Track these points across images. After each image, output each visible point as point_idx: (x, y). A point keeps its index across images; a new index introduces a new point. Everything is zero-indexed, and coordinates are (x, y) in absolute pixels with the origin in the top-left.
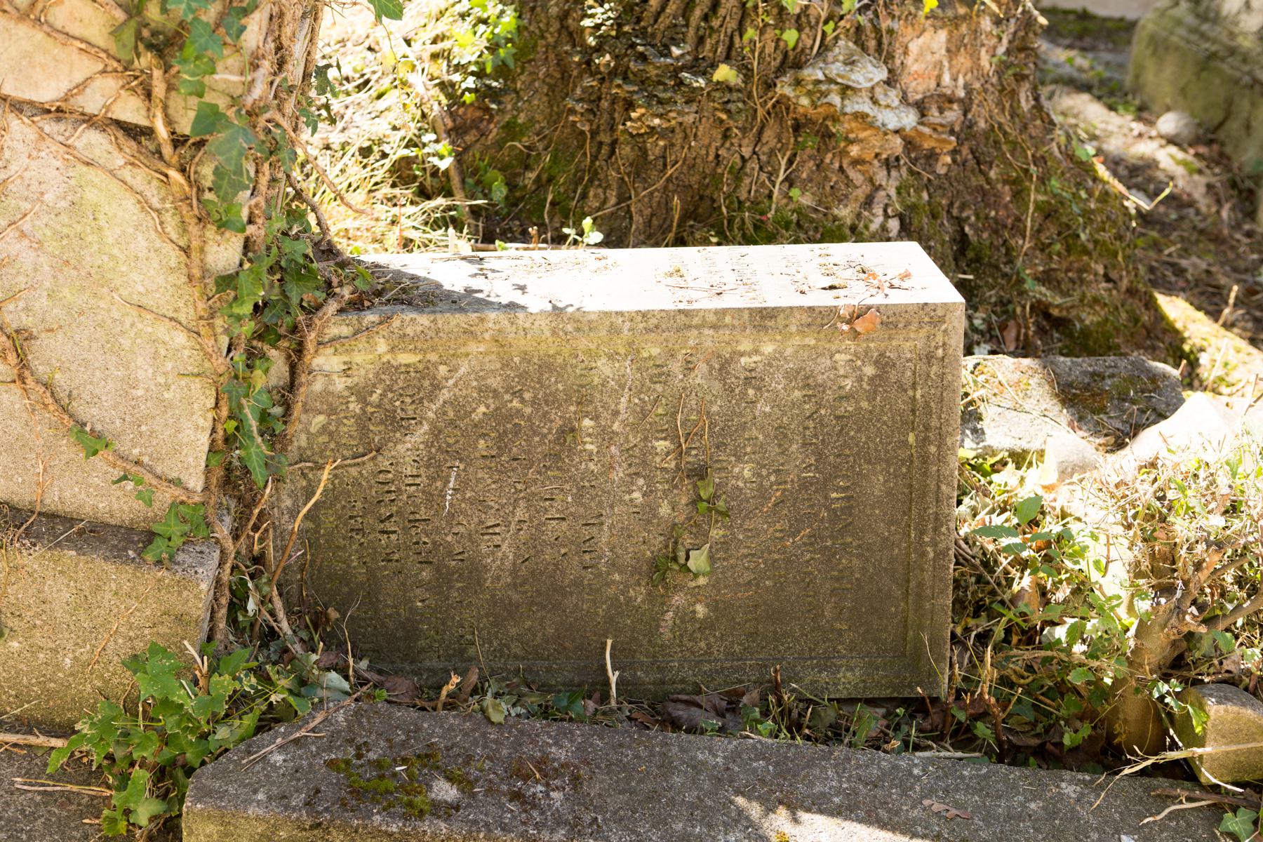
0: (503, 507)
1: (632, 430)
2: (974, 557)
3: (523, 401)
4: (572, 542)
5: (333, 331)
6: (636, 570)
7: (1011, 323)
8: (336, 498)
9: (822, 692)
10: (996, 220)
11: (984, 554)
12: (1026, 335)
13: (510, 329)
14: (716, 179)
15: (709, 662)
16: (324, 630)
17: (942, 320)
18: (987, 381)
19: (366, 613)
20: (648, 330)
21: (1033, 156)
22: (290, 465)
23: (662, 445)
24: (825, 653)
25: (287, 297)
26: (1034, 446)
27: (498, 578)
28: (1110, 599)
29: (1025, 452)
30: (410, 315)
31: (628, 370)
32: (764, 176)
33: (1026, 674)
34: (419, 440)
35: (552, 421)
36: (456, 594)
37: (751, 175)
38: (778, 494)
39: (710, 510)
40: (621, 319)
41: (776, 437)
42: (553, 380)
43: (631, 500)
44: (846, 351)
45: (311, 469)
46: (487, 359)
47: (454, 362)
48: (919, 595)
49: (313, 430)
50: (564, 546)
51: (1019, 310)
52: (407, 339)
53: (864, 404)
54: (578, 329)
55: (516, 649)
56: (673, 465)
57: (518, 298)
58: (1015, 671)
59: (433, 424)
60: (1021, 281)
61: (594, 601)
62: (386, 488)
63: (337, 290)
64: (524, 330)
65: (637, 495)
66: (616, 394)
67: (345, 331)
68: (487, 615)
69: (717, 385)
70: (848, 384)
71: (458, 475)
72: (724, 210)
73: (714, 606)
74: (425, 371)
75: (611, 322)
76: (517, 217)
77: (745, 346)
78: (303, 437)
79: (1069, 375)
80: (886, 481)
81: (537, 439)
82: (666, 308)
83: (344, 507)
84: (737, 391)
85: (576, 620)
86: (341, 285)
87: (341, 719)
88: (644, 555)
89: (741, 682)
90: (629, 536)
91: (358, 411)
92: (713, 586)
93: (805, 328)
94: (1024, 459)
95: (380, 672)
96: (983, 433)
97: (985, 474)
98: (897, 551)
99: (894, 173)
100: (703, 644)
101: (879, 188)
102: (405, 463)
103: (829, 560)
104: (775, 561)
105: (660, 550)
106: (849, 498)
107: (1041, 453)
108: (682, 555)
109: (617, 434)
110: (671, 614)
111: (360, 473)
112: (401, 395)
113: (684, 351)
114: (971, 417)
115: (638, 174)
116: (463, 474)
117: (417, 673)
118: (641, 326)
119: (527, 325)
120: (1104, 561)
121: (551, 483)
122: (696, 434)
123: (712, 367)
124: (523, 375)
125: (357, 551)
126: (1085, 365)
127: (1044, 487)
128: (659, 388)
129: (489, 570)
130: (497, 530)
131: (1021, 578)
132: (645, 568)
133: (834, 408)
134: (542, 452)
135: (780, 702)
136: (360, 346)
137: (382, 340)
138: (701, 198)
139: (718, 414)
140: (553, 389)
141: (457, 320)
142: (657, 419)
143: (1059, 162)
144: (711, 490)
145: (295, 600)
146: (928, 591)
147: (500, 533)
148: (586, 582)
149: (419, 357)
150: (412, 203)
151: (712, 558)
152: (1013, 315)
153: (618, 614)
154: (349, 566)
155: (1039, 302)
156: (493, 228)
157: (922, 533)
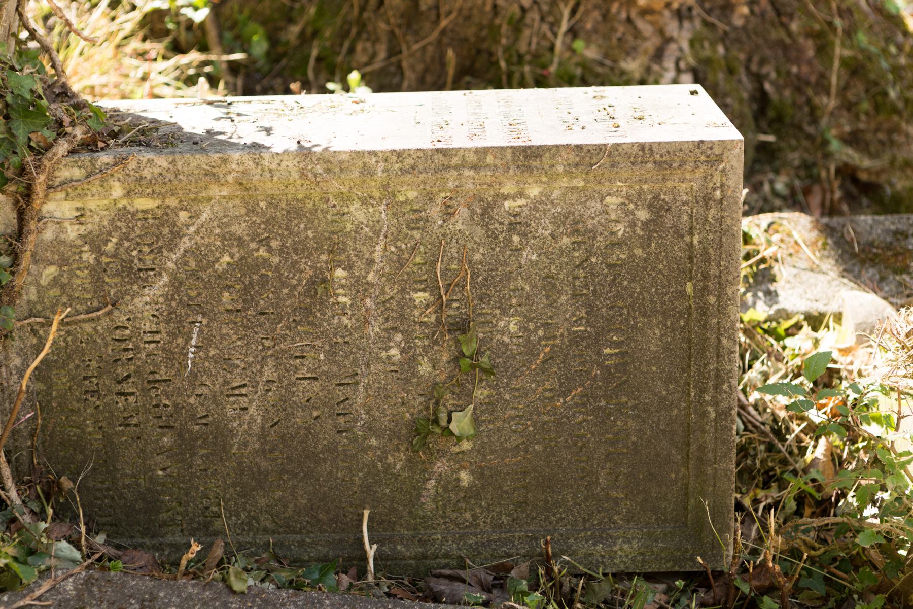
0: (250, 365)
1: (388, 280)
2: (763, 424)
3: (270, 250)
4: (325, 404)
5: (65, 173)
6: (394, 434)
7: (816, 189)
8: (69, 357)
9: (598, 567)
10: (798, 77)
11: (775, 421)
12: (832, 201)
13: (255, 171)
14: (494, 31)
15: (475, 535)
16: (57, 502)
17: (719, 159)
18: (782, 241)
19: (102, 482)
20: (404, 171)
21: (839, 8)
22: (19, 320)
23: (420, 297)
24: (599, 524)
25: (13, 135)
26: (832, 308)
27: (245, 444)
28: (901, 455)
29: (822, 315)
30: (147, 155)
31: (383, 216)
32: (545, 28)
33: (816, 545)
34: (158, 293)
35: (301, 272)
36: (200, 462)
37: (532, 26)
38: (547, 350)
39: (473, 367)
40: (374, 160)
41: (543, 288)
42: (302, 226)
43: (389, 358)
44: (617, 194)
45: (42, 325)
46: (231, 204)
47: (195, 207)
48: (700, 459)
49: (43, 282)
50: (317, 408)
51: (824, 174)
52: (144, 182)
53: (638, 252)
54: (328, 171)
55: (266, 521)
56: (433, 318)
57: (262, 138)
58: (805, 542)
59: (173, 275)
60: (825, 143)
61: (350, 469)
62: (123, 346)
63: (69, 130)
64: (270, 171)
65: (394, 352)
66: (371, 242)
67: (77, 173)
68: (234, 485)
69: (480, 232)
70: (621, 229)
71: (201, 331)
72: (503, 64)
73: (479, 473)
74: (165, 218)
75: (363, 163)
76: (279, 74)
77: (509, 188)
78: (33, 289)
79: (870, 233)
80: (662, 336)
81: (286, 291)
82: (423, 147)
83: (78, 367)
84: (501, 238)
85: (331, 489)
86: (73, 124)
87: (70, 587)
88: (403, 418)
89: (509, 555)
90: (387, 397)
91: (92, 262)
92: (479, 451)
93: (571, 169)
94: (821, 323)
95: (118, 547)
96: (777, 295)
97: (778, 338)
98: (675, 411)
99: (686, 24)
100: (468, 515)
101: (669, 40)
102: (143, 318)
103: (603, 422)
104: (545, 423)
105: (420, 411)
106: (623, 354)
107: (838, 317)
108: (443, 416)
109: (372, 285)
110: (433, 482)
111: (95, 329)
112: (138, 244)
113: (443, 195)
114: (763, 278)
115: (409, 26)
116: (206, 330)
117: (159, 548)
118: (396, 166)
119: (274, 166)
120: (895, 417)
121: (302, 340)
122: (457, 285)
123: (473, 212)
124: (270, 222)
125: (92, 415)
126: (887, 223)
127: (841, 350)
128: (417, 234)
129: (236, 435)
130: (244, 391)
131: (815, 447)
132: (404, 432)
133: (605, 256)
134: (291, 306)
135: (549, 571)
136: (94, 190)
137: (117, 184)
138: (479, 52)
139: (481, 263)
140: (303, 236)
141: (199, 161)
142: (415, 269)
143: (866, 16)
144: (475, 345)
145: (25, 468)
146: (710, 455)
147: (246, 393)
148: (340, 448)
149: (158, 202)
150: (165, 58)
151: (476, 421)
152: (817, 180)
153: (376, 482)
154: (84, 432)
155: (846, 165)
156: (252, 80)
157: (703, 391)
